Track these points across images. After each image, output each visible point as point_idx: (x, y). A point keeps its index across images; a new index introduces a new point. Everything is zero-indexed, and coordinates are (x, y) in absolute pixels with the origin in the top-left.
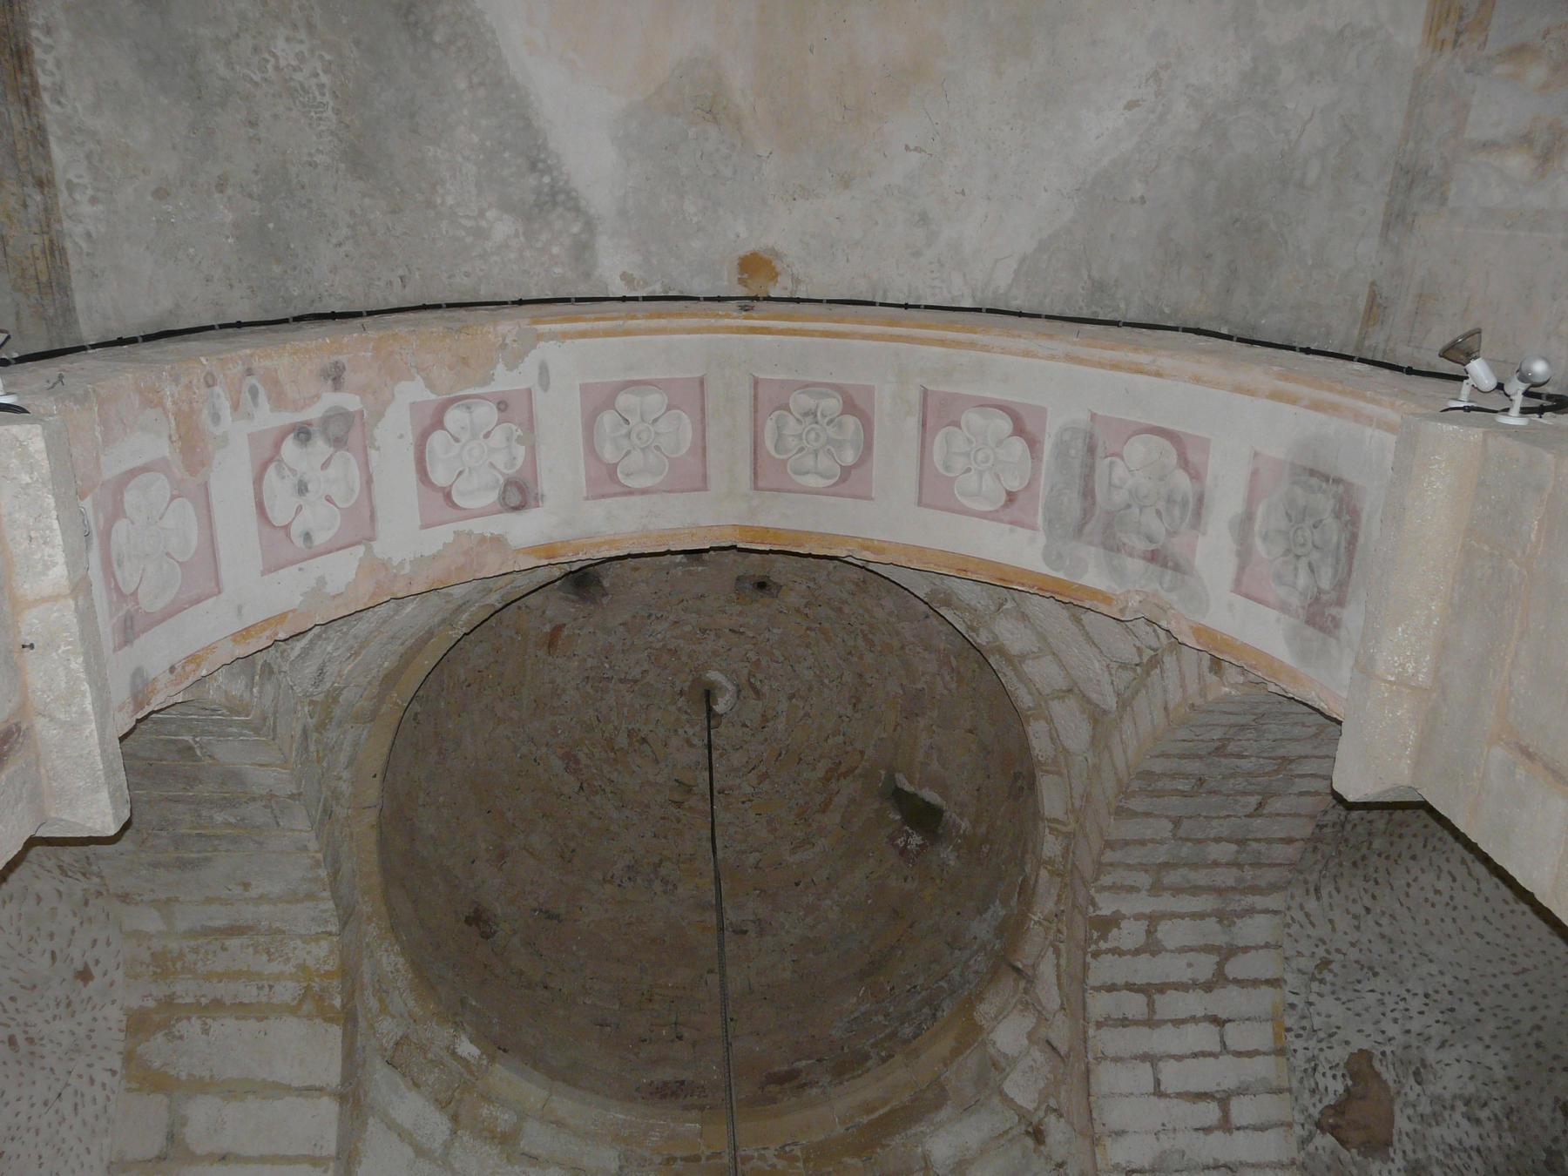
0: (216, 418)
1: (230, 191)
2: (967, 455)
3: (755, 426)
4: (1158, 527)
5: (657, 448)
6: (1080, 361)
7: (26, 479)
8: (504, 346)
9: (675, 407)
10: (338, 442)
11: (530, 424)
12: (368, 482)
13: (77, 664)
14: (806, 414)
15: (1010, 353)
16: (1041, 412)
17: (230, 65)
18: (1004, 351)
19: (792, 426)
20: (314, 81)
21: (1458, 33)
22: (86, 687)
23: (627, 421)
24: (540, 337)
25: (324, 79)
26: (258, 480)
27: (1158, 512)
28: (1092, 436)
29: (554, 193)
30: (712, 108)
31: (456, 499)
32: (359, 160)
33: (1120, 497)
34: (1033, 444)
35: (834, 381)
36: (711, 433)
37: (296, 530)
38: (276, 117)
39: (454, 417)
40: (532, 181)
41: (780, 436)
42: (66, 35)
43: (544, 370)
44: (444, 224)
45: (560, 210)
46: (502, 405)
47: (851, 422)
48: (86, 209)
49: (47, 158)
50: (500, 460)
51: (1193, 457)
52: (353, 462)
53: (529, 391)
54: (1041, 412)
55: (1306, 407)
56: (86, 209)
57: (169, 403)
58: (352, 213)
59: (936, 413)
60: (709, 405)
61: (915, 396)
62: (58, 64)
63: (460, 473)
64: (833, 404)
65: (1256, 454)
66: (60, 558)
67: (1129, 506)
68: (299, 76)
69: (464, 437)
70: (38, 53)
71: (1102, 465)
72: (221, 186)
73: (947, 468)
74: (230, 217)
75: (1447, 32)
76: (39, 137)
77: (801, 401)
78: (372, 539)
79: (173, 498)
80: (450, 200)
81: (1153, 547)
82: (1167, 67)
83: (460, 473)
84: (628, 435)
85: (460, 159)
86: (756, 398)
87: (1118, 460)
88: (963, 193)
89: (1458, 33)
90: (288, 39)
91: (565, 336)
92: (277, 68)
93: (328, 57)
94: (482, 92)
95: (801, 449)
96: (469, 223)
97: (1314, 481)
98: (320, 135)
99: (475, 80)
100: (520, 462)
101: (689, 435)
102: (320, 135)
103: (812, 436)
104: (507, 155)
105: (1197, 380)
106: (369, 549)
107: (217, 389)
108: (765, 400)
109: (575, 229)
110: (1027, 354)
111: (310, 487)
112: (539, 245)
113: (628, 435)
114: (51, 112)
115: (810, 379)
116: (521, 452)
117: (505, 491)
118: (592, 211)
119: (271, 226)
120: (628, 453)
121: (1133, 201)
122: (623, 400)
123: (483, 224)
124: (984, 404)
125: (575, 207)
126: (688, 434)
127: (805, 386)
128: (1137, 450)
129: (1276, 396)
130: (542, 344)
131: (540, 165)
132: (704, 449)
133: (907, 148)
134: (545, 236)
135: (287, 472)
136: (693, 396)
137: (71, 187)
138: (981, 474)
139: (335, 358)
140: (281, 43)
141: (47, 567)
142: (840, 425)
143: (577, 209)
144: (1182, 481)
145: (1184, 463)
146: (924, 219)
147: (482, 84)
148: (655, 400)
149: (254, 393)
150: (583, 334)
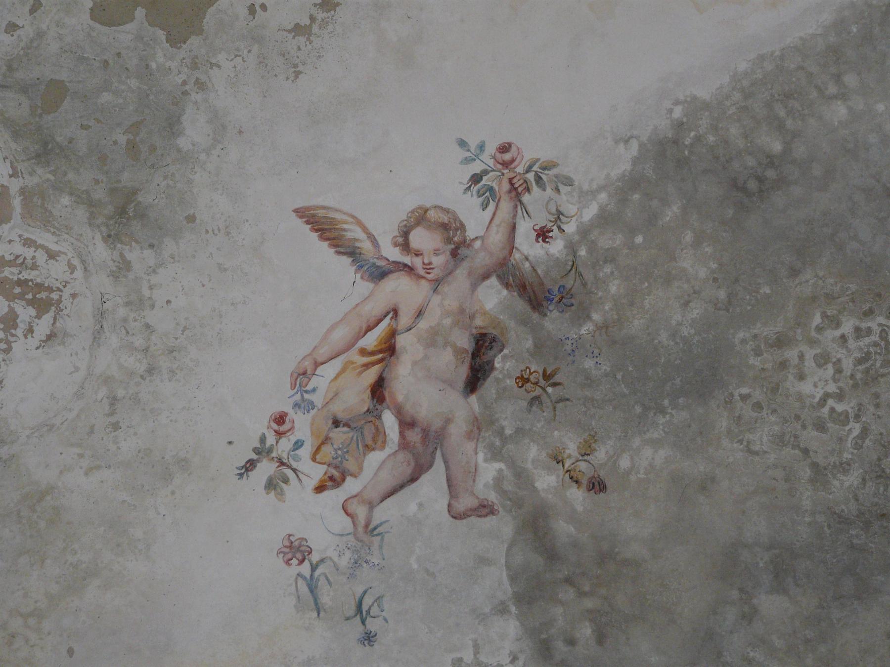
17: (844, 467)
20: (852, 344)
25: (847, 327)
68: (848, 365)
90: (801, 377)
92: (840, 396)
93: (817, 320)
94: (851, 80)
99: (832, 89)
140: (806, 387)
147: (838, 78)
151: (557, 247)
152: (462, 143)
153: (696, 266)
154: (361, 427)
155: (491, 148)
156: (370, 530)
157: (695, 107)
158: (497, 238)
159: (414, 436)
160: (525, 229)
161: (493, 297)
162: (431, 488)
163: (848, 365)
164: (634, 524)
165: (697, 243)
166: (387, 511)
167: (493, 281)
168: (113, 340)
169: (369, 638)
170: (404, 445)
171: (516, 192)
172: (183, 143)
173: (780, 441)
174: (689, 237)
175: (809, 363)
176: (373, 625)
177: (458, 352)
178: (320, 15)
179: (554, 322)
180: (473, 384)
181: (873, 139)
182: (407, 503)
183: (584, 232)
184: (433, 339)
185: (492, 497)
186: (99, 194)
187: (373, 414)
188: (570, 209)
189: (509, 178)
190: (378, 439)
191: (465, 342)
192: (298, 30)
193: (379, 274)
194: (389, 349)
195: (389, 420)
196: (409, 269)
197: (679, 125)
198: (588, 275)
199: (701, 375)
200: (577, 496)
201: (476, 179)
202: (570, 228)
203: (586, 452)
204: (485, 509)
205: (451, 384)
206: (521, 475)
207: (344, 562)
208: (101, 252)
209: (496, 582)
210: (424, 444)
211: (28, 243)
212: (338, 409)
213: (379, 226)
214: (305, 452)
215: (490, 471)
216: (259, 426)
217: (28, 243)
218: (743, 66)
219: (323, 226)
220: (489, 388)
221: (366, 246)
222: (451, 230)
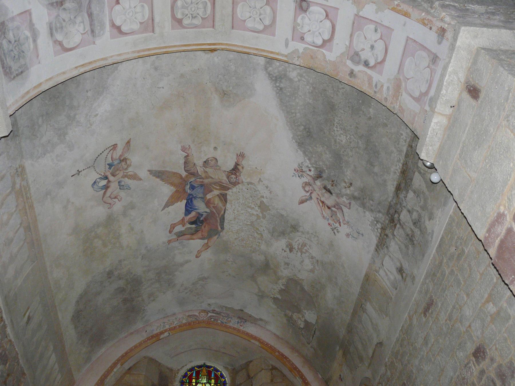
0: (388, 88)
1: (368, 116)
2: (136, 13)
3: (214, 11)
4: (64, 15)
5: (250, 7)
6: (102, 59)
7: (430, 148)
8: (299, 57)
9: (242, 20)
10: (357, 54)
11: (294, 29)
12: (351, 36)
13: (444, 92)
14: (196, 17)
15: (126, 53)
16: (112, 37)
17: (358, 143)
18: (128, 53)
19: (201, 12)
20: (338, 129)
21: (17, 171)
22: (445, 83)
23: (260, 19)
24: (286, 56)
25: (335, 129)
26: (383, 61)
27: (64, 21)
28: (93, 36)
29: (276, 80)
30: (224, 94)
31: (325, 14)
32: (332, 107)
33: (79, 19)
34: (113, 25)
35: (186, 30)
36: (230, 9)
37: (379, 36)
38: (351, 126)
39: (319, 42)
40: (282, 85)
41: (205, 8)
42: (392, 169)
43: (287, 45)
44: (311, 82)
45: (275, 75)
46: (302, 39)
47: (179, 16)
48: (404, 134)
49: (407, 151)
50: (307, 20)
51: (59, 47)
52: (354, 45)
53: (293, 40)
54: (112, 37)
55: (30, 90)
56: (404, 134)
57: (398, 104)
58: (337, 95)
59: (149, 25)
60: (230, 18)
61: (157, 29)
62: (396, 165)
63: (321, 22)
64: (186, 22)
65: (39, 63)
66: (432, 124)
67: (75, 17)
68: (342, 132)
69: (317, 33)
70: (399, 170)
71: (88, 28)
72: (370, 118)
73: (143, 6)
74: (371, 110)
75: (20, 170)
76: (407, 156)
77: (196, 22)
78: (356, 15)
79: (408, 79)
80: (308, 87)
81: (63, 7)
82: (89, 128)
83: (321, 22)
84: (260, 15)
85: (303, 97)
86: (214, 21)
87: (82, 32)
88: (144, 78)
89: (17, 171)
90: (342, 141)
91: (278, 54)
92: (347, 137)
94: (293, 111)
95: (197, 4)
96: (303, 79)
97: (20, 70)
98: (340, 117)
99: (294, 115)
100: (300, 17)
101: (238, 9)
102: (340, 117)
103: (193, 9)
104: (288, 94)
105: (64, 73)
106: (358, 12)
107: (385, 96)
108: (211, 21)
109: (270, 69)
110: (120, 55)
111: (370, 46)
112: (283, 67)
113: (260, 15)
114: (402, 158)
115: (194, 30)
116: (299, 21)
117: (307, 9)
118: (264, 72)
119: (361, 102)
120: (261, 8)
121: (90, 90)
122: (261, 27)
123: (299, 78)
124: (132, 33)
125: (270, 76)
126: (239, 9)
127: (196, 27)
128: (77, 39)
129: (40, 84)
130: (286, 54)
131: (279, 89)
132: (233, 3)
133: (163, 88)
134: (281, 69)
135: (375, 56)
136: (236, 23)
137: (405, 141)
138: (130, 7)
139: (351, 79)
140: (344, 141)
141: (437, 123)
142: (183, 14)
143: (269, 74)
144: (59, 37)
145: (60, 44)
146: (156, 69)
147: (292, 113)
148: (250, 24)
149: (376, 85)
150: (272, 53)
151: (312, 169)
152: (293, 176)
153: (320, 149)
154: (333, 214)
155: (295, 172)
156: (348, 222)
157: (293, 138)
158: (309, 177)
159: (337, 207)
160: (309, 173)
161: (318, 183)
162: (345, 209)
163: (342, 132)
164: (358, 184)
165: (316, 147)
166: (346, 218)
167: (316, 181)
168: (312, 239)
169: (362, 235)
170: (337, 209)
171: (302, 171)
172: (285, 215)
173: (351, 151)
174: (315, 148)
175: (340, 138)
176: (361, 233)
177: (325, 192)
178: (269, 189)
179: (325, 175)
180: (331, 194)
181: (304, 111)
182: (346, 215)
183: (311, 164)
184: (323, 196)
185: (348, 201)
186: (291, 230)
187: (332, 210)
188: (307, 164)
189: (300, 171)
190: (335, 212)
191: (324, 191)
192: (270, 193)
193: (311, 198)
194: (323, 202)
195: (333, 209)
196: (311, 193)
197: (296, 142)
198: (318, 167)
199: (338, 157)
200: (351, 188)
201: (299, 176)
202: (310, 166)
203: (345, 182)
204: (350, 203)
205: (330, 197)
206: (347, 195)
207: (351, 230)
208: (300, 234)
209: (361, 209)
210: (337, 205)
211: (296, 242)
212: (330, 215)
213: (302, 194)
214: (335, 224)
215: (344, 199)
216: (329, 228)
217: (296, 242)
218: (288, 128)
219: (302, 202)
220: (332, 191)
221: (306, 197)
222: (307, 184)
